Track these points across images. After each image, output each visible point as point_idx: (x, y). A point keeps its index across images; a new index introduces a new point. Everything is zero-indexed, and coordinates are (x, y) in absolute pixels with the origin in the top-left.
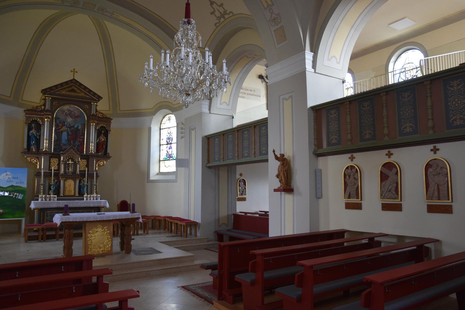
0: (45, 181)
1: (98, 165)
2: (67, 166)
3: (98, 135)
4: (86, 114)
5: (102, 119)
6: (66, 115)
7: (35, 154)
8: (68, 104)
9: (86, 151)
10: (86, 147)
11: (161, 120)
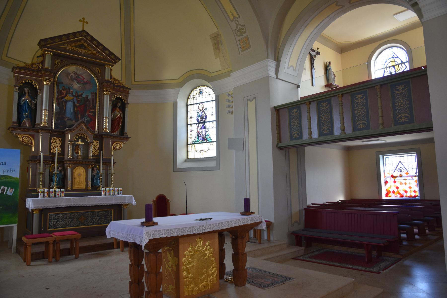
0: (44, 169)
1: (114, 148)
2: (75, 147)
3: (113, 109)
4: (98, 79)
5: (118, 88)
6: (72, 79)
7: (29, 129)
8: (75, 64)
9: (98, 129)
10: (98, 124)
11: (188, 93)
